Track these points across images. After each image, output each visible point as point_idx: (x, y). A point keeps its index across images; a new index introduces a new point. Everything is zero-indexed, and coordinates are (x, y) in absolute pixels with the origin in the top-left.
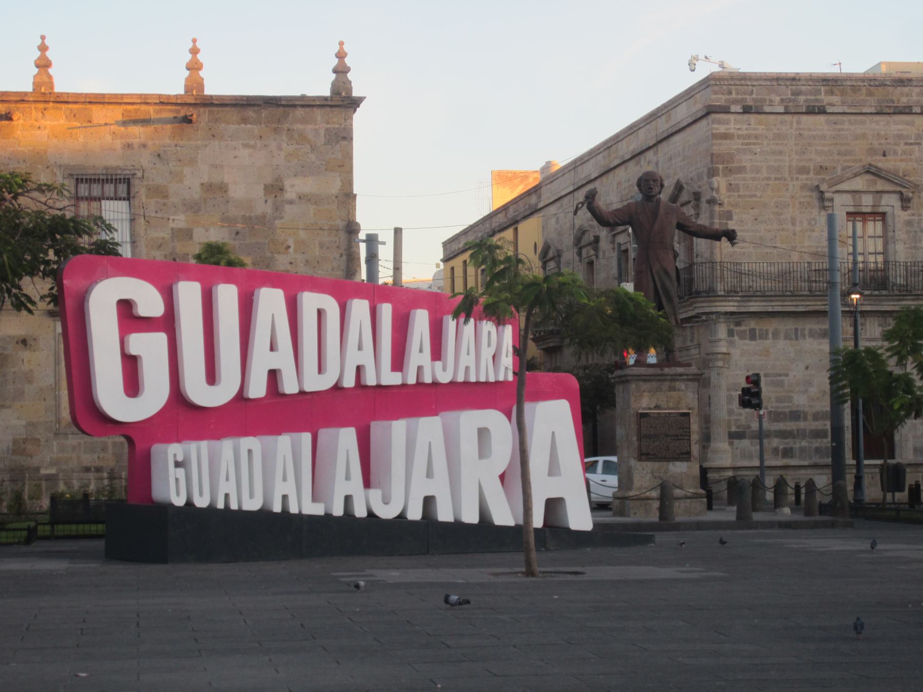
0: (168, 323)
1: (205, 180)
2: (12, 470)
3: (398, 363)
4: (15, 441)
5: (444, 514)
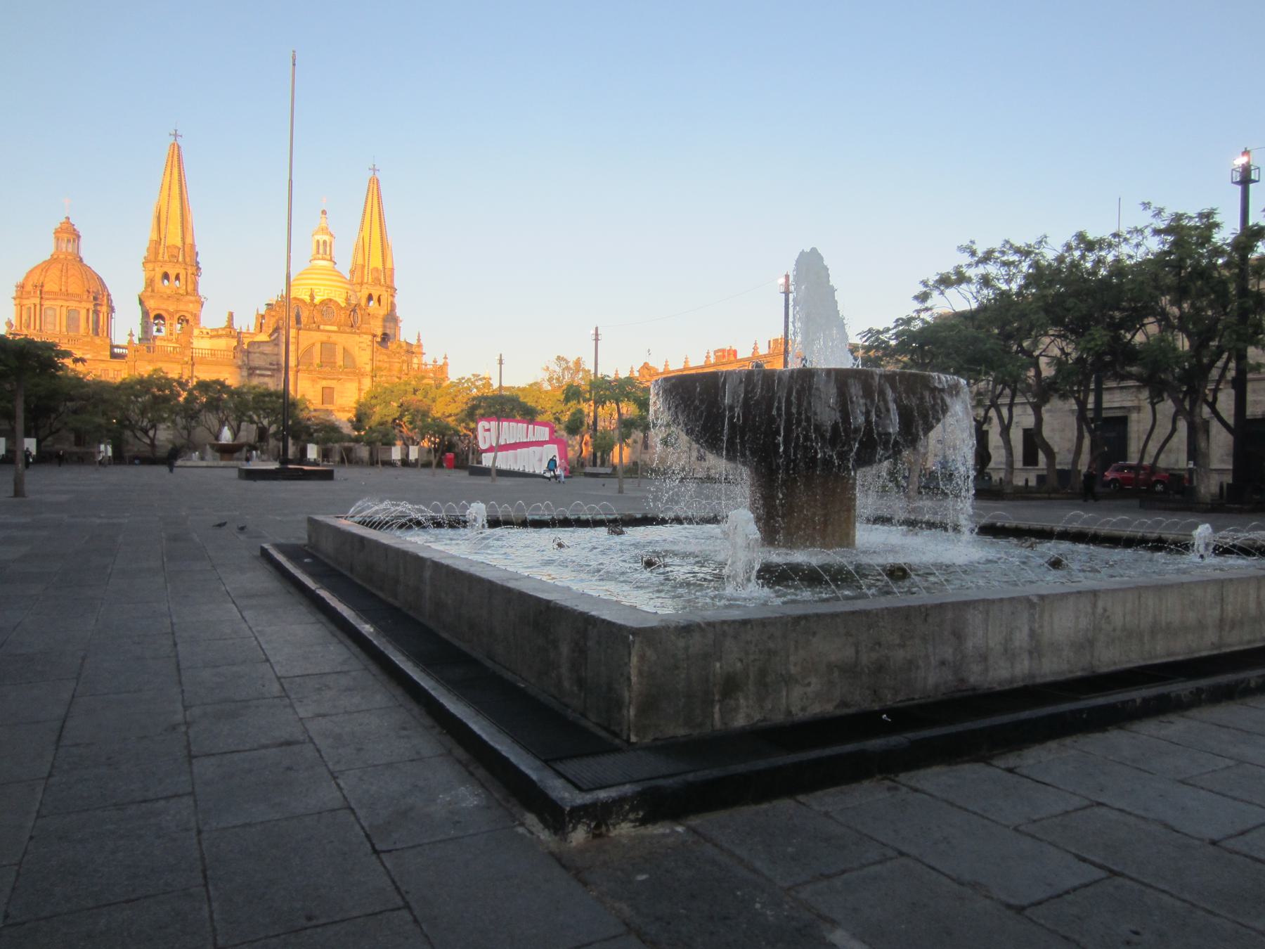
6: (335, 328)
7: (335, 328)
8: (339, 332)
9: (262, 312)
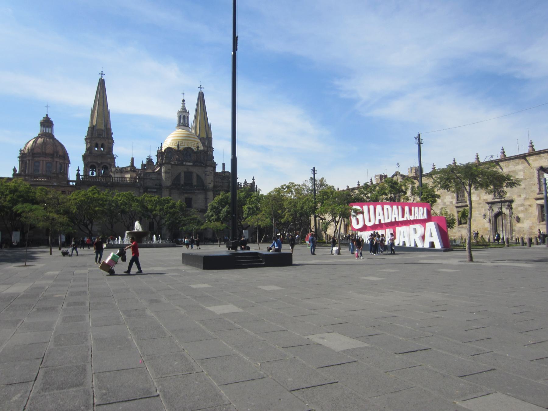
0: (362, 213)
3: (403, 216)
5: (407, 245)
6: (191, 164)
7: (191, 164)
8: (194, 165)
9: (145, 162)
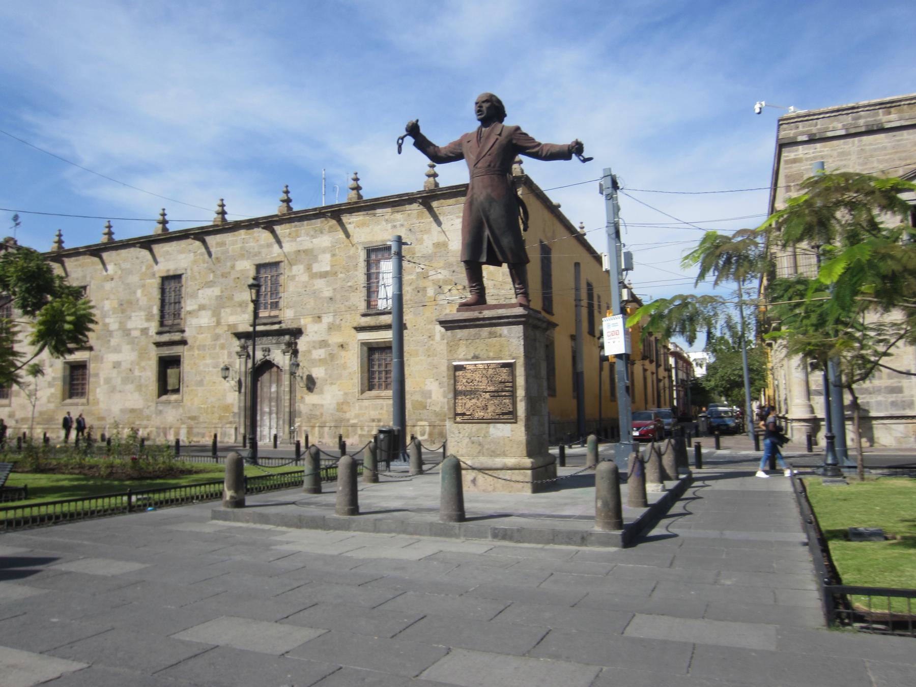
1: (435, 241)
2: (336, 421)
4: (338, 404)
